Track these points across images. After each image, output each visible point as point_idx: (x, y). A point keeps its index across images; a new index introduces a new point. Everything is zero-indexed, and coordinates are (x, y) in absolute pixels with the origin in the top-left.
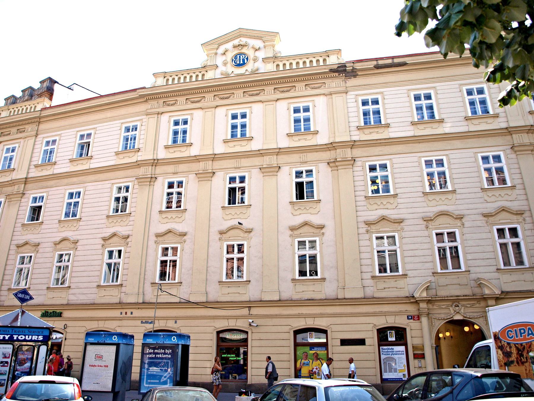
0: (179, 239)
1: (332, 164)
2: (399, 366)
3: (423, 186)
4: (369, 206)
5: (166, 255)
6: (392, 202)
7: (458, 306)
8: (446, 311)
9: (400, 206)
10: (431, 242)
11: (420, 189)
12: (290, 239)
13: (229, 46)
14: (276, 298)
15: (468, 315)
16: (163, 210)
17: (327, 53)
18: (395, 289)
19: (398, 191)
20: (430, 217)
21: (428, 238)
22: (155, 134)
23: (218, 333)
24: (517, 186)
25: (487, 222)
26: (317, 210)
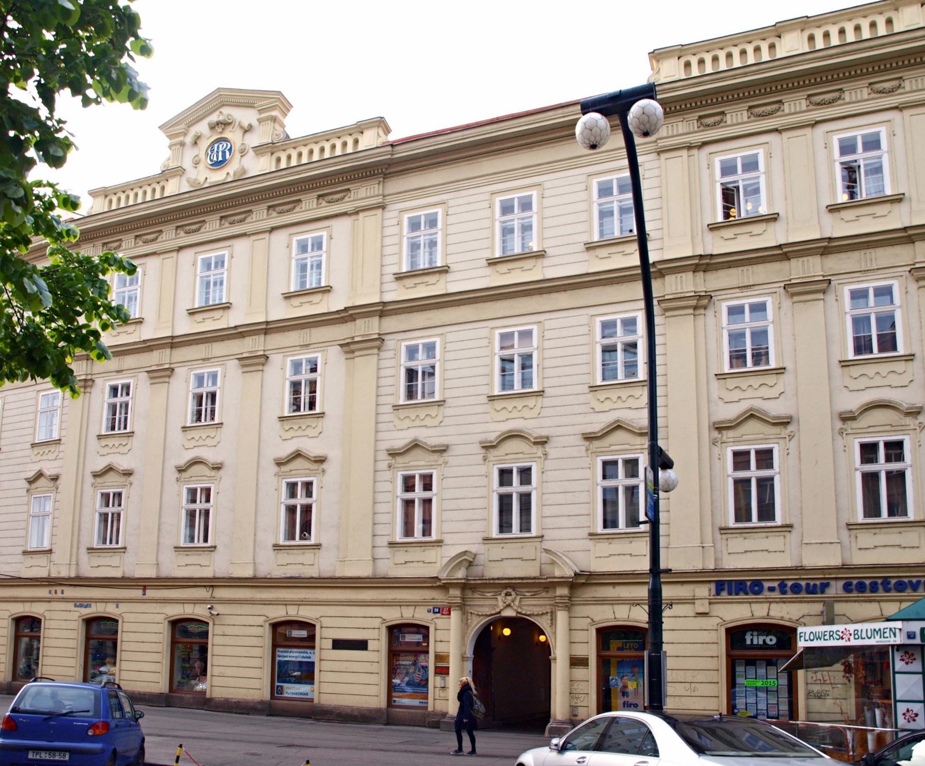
1: (349, 347)
3: (591, 373)
4: (397, 422)
5: (874, 460)
6: (433, 414)
8: (493, 602)
9: (447, 421)
11: (586, 379)
12: (275, 480)
13: (202, 127)
14: (248, 573)
15: (526, 610)
16: (188, 425)
17: (360, 128)
18: (421, 564)
19: (448, 394)
20: (491, 442)
25: (587, 450)
26: (128, 447)
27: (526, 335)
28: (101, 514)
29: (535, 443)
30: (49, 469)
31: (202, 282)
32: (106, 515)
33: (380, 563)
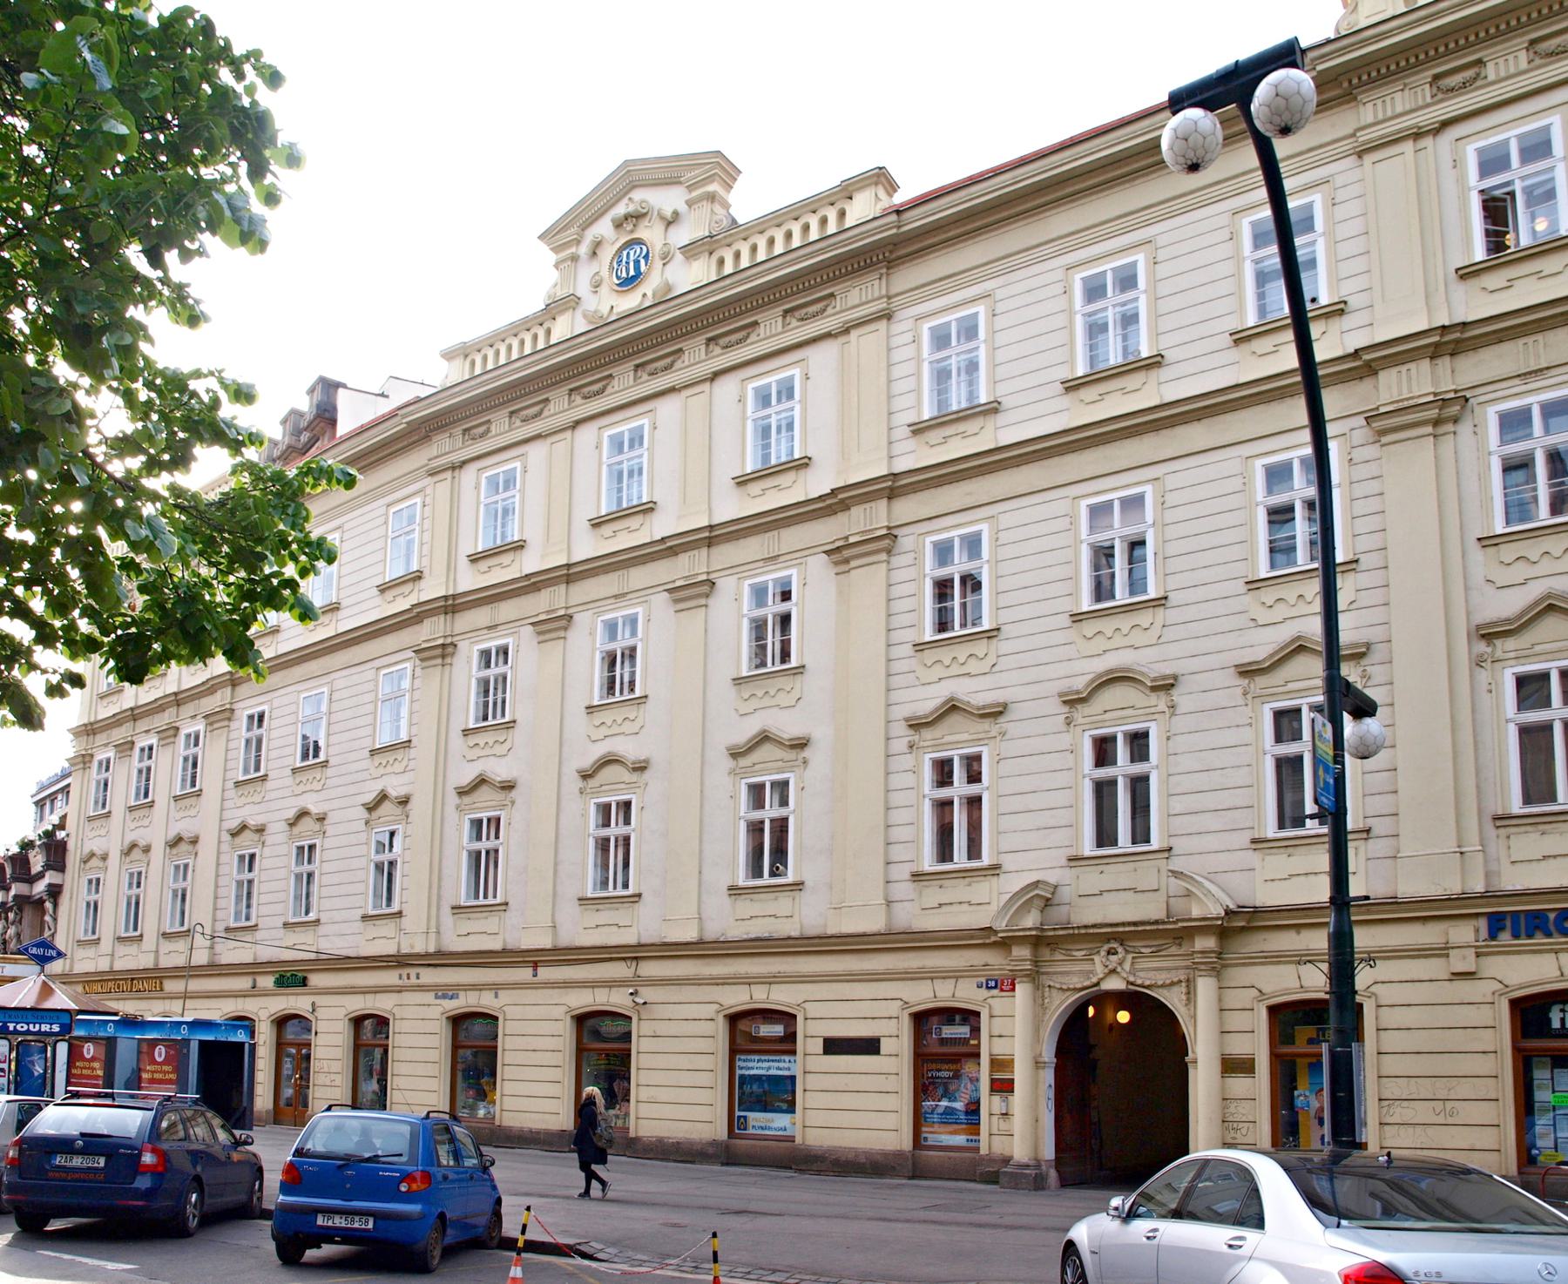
0: (500, 796)
1: (841, 554)
4: (921, 672)
8: (1086, 967)
9: (1004, 663)
11: (1240, 569)
13: (604, 228)
16: (745, 674)
20: (1078, 692)
22: (1196, 276)
23: (734, 1019)
24: (1363, 558)
25: (1245, 694)
26: (507, 745)
28: (470, 853)
29: (1154, 689)
30: (396, 789)
31: (610, 473)
32: (479, 853)
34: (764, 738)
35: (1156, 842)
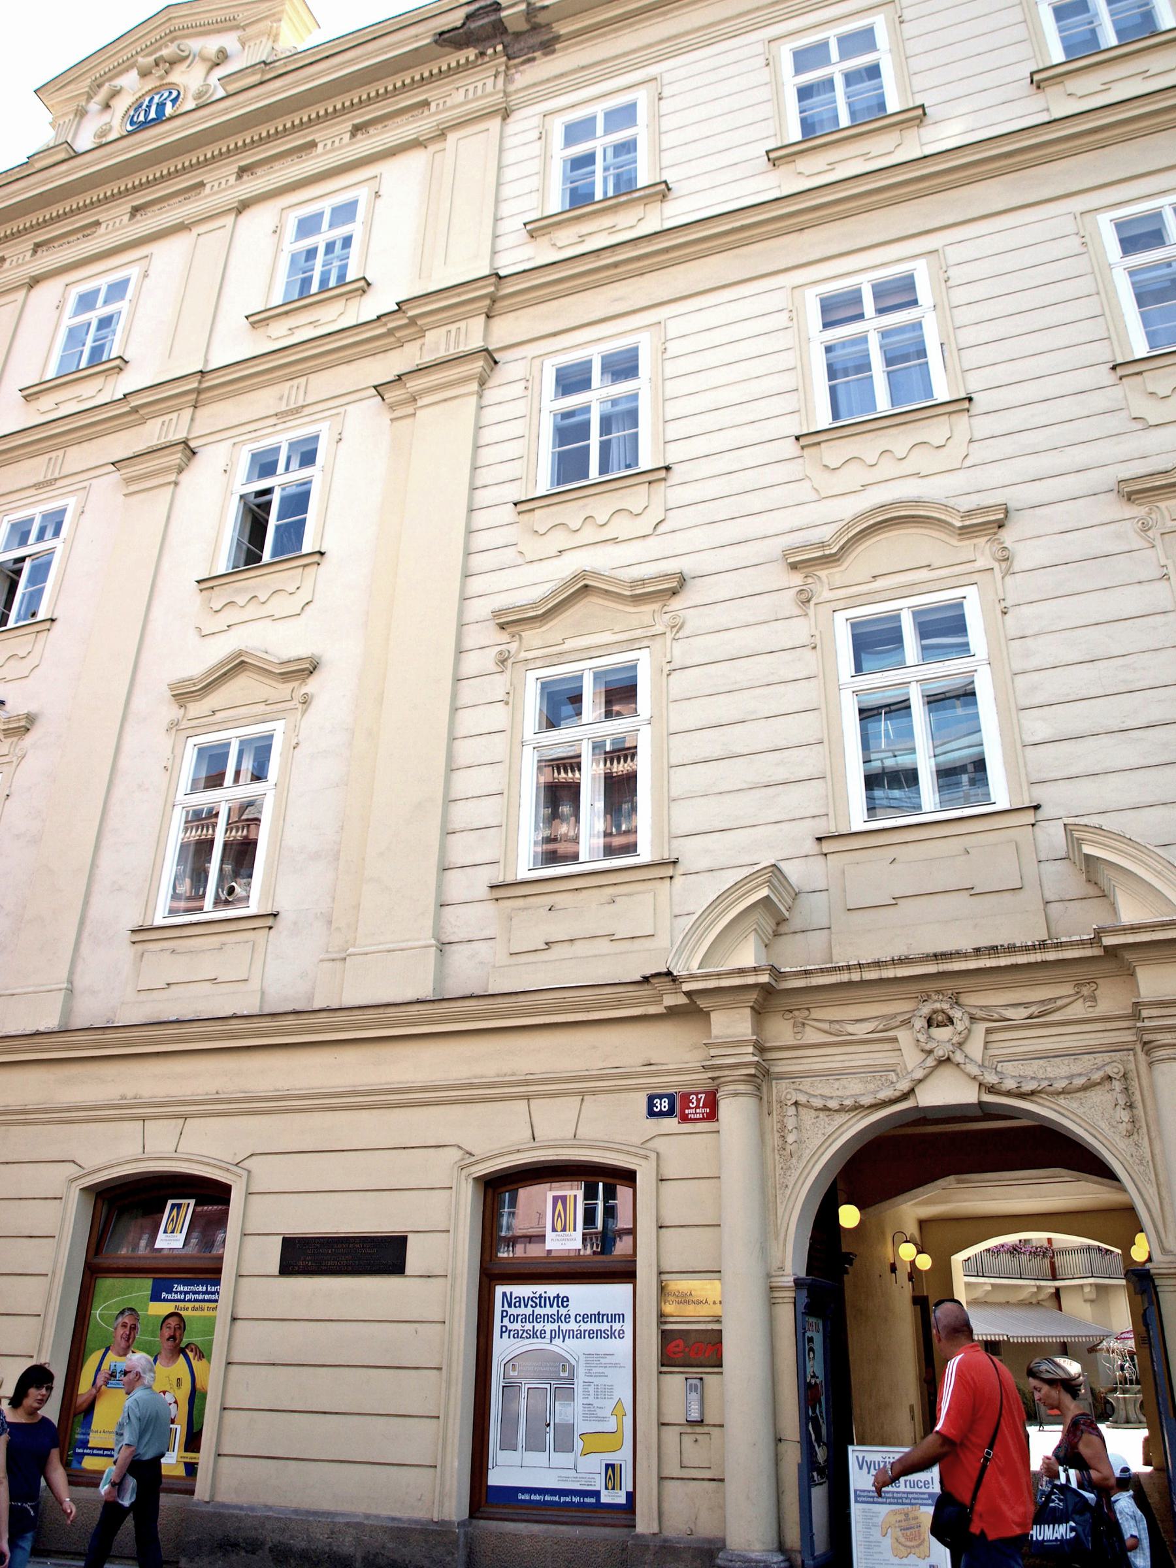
2: (591, 1413)
7: (951, 1021)
8: (879, 1056)
10: (824, 677)
11: (1102, 352)
12: (165, 742)
18: (604, 946)
20: (822, 545)
21: (807, 653)
25: (1145, 528)
27: (898, 294)
29: (966, 532)
33: (459, 957)
34: (238, 665)
35: (645, 853)
